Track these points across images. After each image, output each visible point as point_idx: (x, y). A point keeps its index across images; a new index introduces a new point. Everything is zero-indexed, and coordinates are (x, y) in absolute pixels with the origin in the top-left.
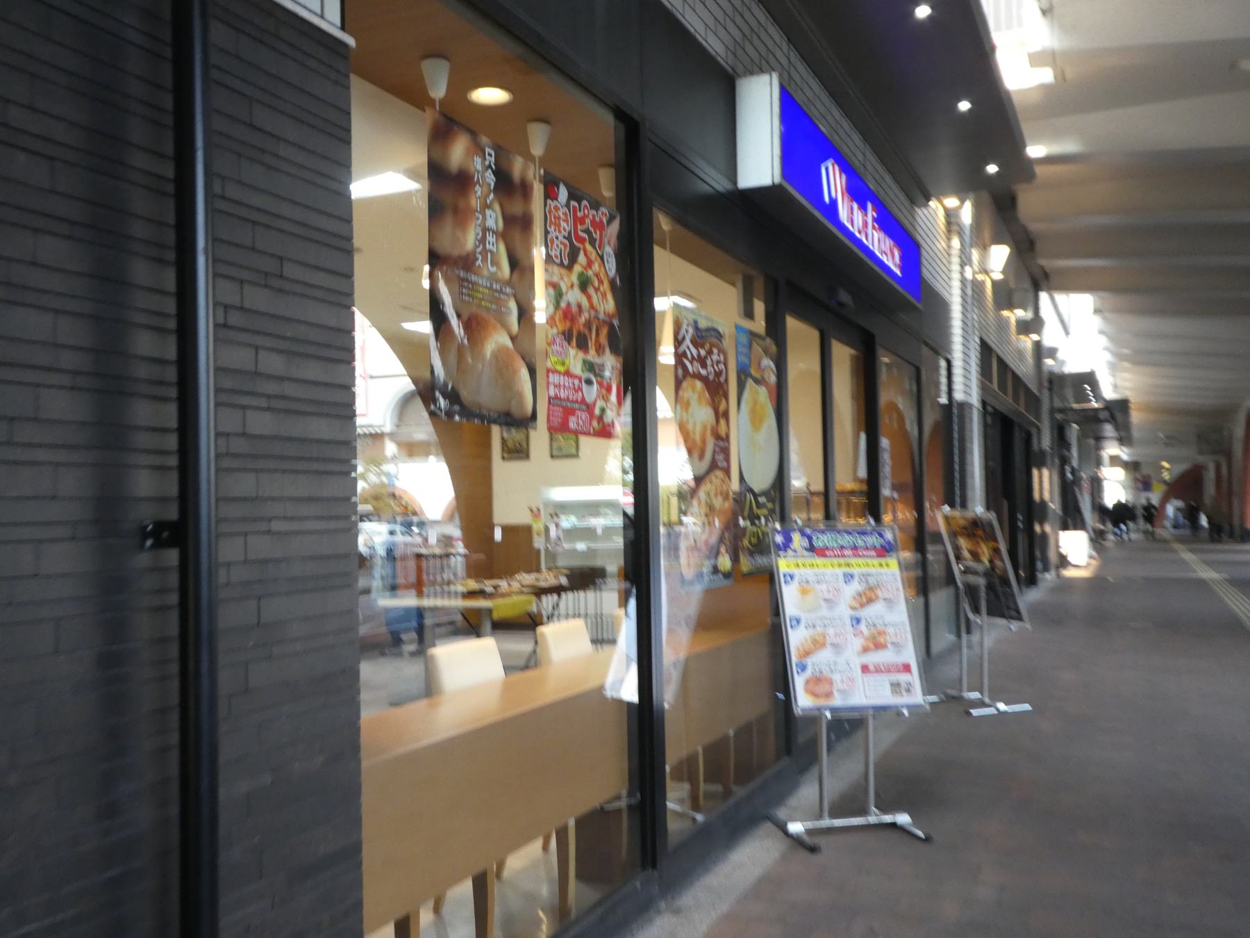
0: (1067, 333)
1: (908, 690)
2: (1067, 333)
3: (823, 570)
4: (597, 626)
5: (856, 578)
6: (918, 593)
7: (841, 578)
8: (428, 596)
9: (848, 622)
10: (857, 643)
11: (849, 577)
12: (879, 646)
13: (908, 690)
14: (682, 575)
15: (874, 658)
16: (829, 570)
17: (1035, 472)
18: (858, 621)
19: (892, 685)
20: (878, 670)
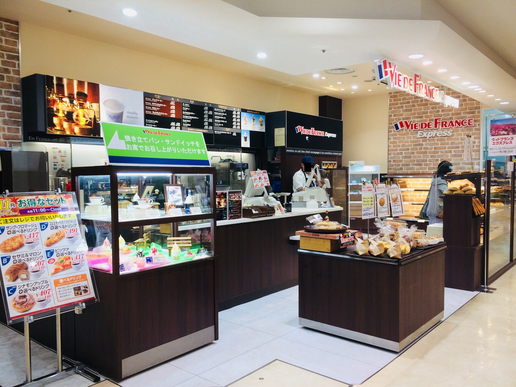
0: (365, 81)
1: (86, 291)
2: (365, 81)
3: (24, 223)
4: (179, 240)
5: (49, 226)
6: (450, 189)
7: (38, 226)
8: (507, 157)
9: (44, 254)
10: (52, 268)
11: (44, 226)
12: (66, 267)
13: (86, 291)
14: (374, 176)
15: (62, 275)
16: (30, 222)
17: (76, 177)
18: (52, 253)
19: (75, 289)
20: (66, 283)
